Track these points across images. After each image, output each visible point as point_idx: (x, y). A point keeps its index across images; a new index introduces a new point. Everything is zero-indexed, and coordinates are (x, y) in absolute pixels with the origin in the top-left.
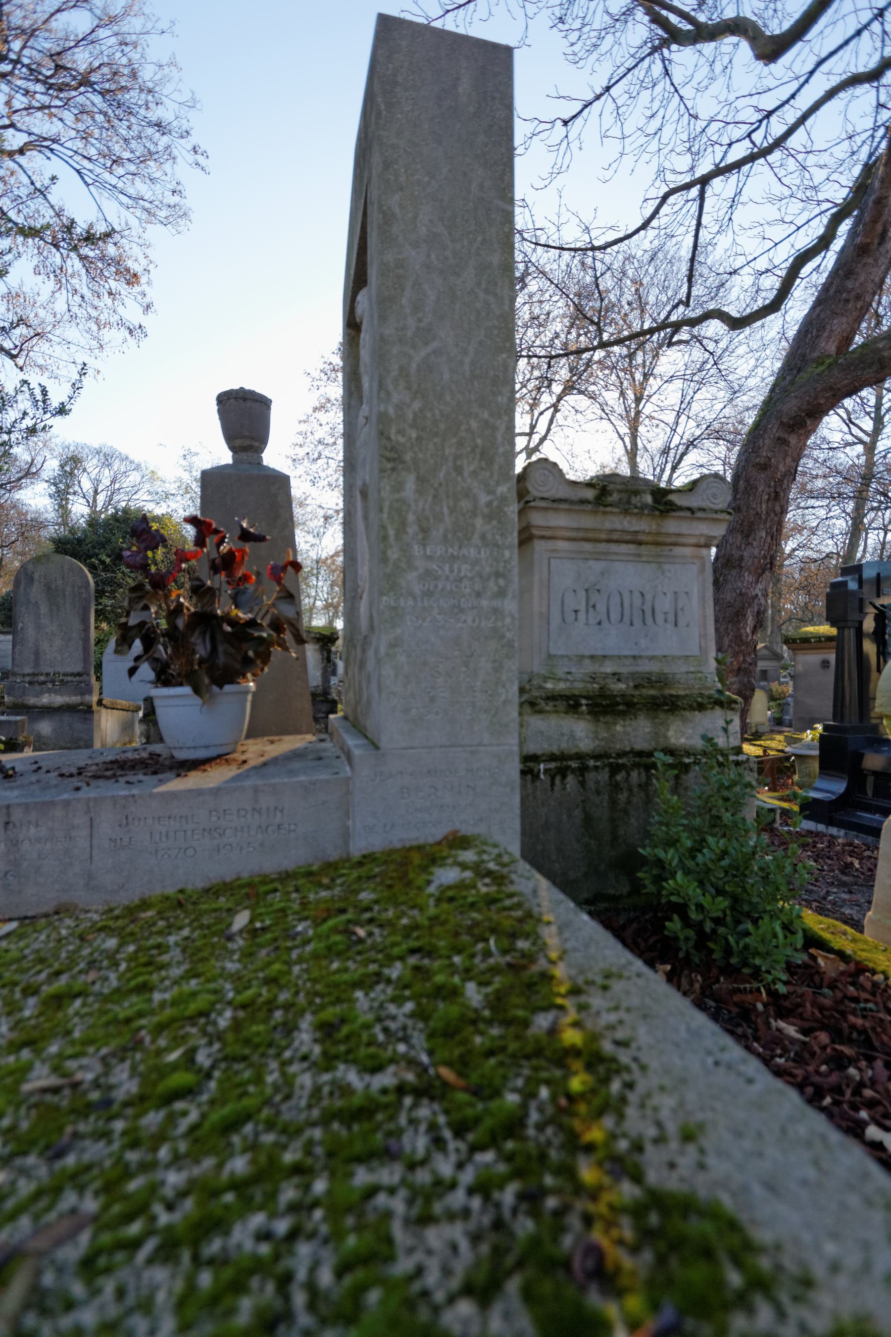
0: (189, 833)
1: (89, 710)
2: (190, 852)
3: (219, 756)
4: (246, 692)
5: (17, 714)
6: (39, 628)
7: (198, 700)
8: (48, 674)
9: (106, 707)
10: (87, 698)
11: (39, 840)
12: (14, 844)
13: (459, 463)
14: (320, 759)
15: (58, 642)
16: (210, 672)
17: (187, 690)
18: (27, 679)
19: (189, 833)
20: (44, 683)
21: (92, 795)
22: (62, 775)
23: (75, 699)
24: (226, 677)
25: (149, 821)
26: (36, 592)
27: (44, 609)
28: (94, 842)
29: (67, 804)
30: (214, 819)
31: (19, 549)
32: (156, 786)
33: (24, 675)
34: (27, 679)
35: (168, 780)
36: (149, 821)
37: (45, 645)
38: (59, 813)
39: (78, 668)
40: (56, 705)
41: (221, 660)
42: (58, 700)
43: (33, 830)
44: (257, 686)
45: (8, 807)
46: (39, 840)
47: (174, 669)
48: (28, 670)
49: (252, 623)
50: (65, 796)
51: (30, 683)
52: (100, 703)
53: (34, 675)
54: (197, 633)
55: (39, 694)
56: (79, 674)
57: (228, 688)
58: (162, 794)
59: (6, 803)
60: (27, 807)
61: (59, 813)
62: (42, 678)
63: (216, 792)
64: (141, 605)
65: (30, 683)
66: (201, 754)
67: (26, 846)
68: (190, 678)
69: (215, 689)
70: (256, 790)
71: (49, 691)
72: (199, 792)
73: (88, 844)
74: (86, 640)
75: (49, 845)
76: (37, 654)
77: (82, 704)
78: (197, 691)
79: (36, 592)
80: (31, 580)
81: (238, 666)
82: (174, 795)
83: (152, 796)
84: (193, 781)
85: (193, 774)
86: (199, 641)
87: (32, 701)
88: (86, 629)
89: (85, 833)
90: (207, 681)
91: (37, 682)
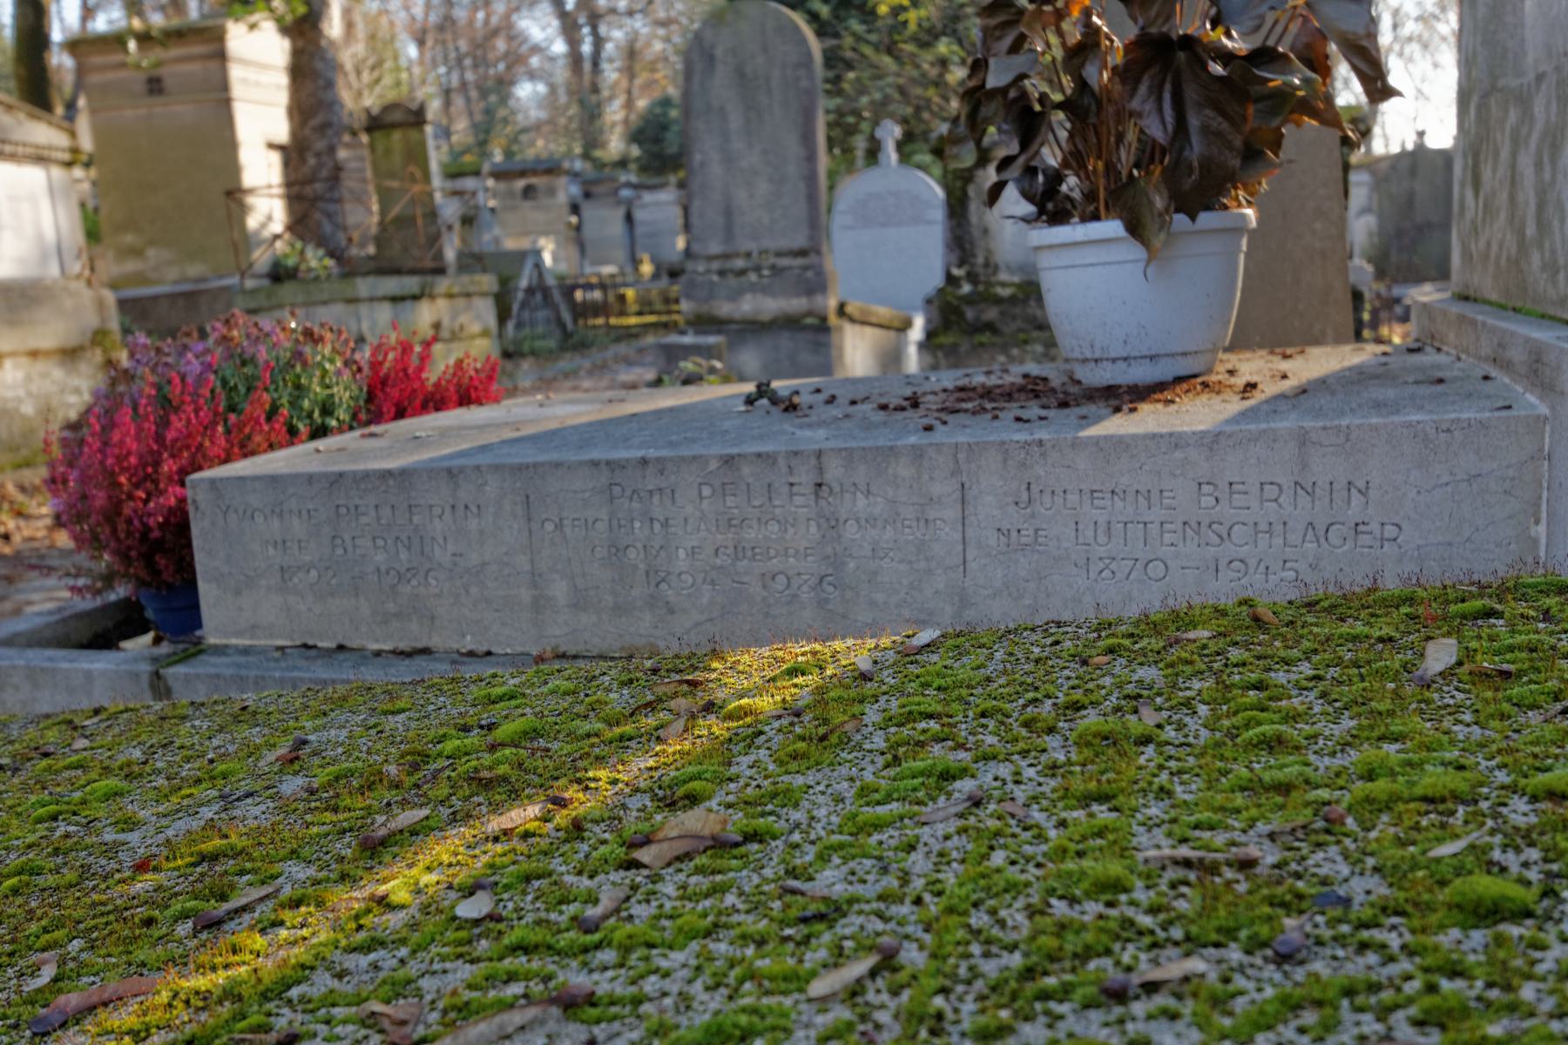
0: (1154, 529)
1: (823, 327)
2: (1156, 569)
3: (1179, 380)
4: (1239, 229)
5: (705, 333)
6: (729, 159)
7: (1135, 251)
8: (748, 255)
9: (852, 320)
10: (819, 300)
11: (872, 521)
12: (832, 524)
13: (660, 66)
14: (1441, 381)
15: (763, 187)
16: (1171, 179)
17: (1112, 227)
18: (716, 265)
19: (1154, 529)
20: (742, 273)
21: (962, 438)
22: (884, 407)
23: (797, 304)
24: (1200, 193)
25: (1073, 498)
26: (721, 86)
27: (735, 121)
28: (970, 532)
29: (918, 454)
30: (1208, 501)
31: (662, 14)
32: (1082, 428)
33: (710, 258)
34: (716, 265)
35: (1098, 419)
36: (1073, 498)
37: (741, 196)
38: (904, 470)
39: (800, 241)
40: (766, 317)
41: (1197, 148)
42: (770, 306)
43: (861, 501)
44: (1260, 220)
45: (819, 454)
46: (872, 521)
47: (1071, 184)
48: (715, 248)
49: (1264, 56)
50: (913, 440)
51: (722, 273)
52: (841, 310)
53: (726, 256)
54: (1143, 89)
55: (735, 296)
56: (802, 253)
57: (1206, 219)
58: (1096, 441)
59: (817, 447)
60: (849, 456)
61: (904, 470)
62: (740, 263)
63: (1212, 441)
64: (1008, 41)
65: (722, 273)
66: (1141, 374)
67: (851, 531)
68: (1116, 198)
69: (1180, 220)
70: (1303, 439)
71: (753, 288)
72: (1175, 441)
73: (958, 536)
74: (811, 179)
75: (889, 533)
76: (728, 213)
77: (809, 314)
78: (1135, 229)
79: (721, 86)
80: (710, 59)
81: (1236, 162)
82: (1120, 444)
83: (1076, 444)
84: (1148, 419)
85: (1145, 408)
86: (1149, 106)
87: (724, 309)
88: (811, 157)
89: (952, 513)
90: (1159, 202)
91: (732, 271)
